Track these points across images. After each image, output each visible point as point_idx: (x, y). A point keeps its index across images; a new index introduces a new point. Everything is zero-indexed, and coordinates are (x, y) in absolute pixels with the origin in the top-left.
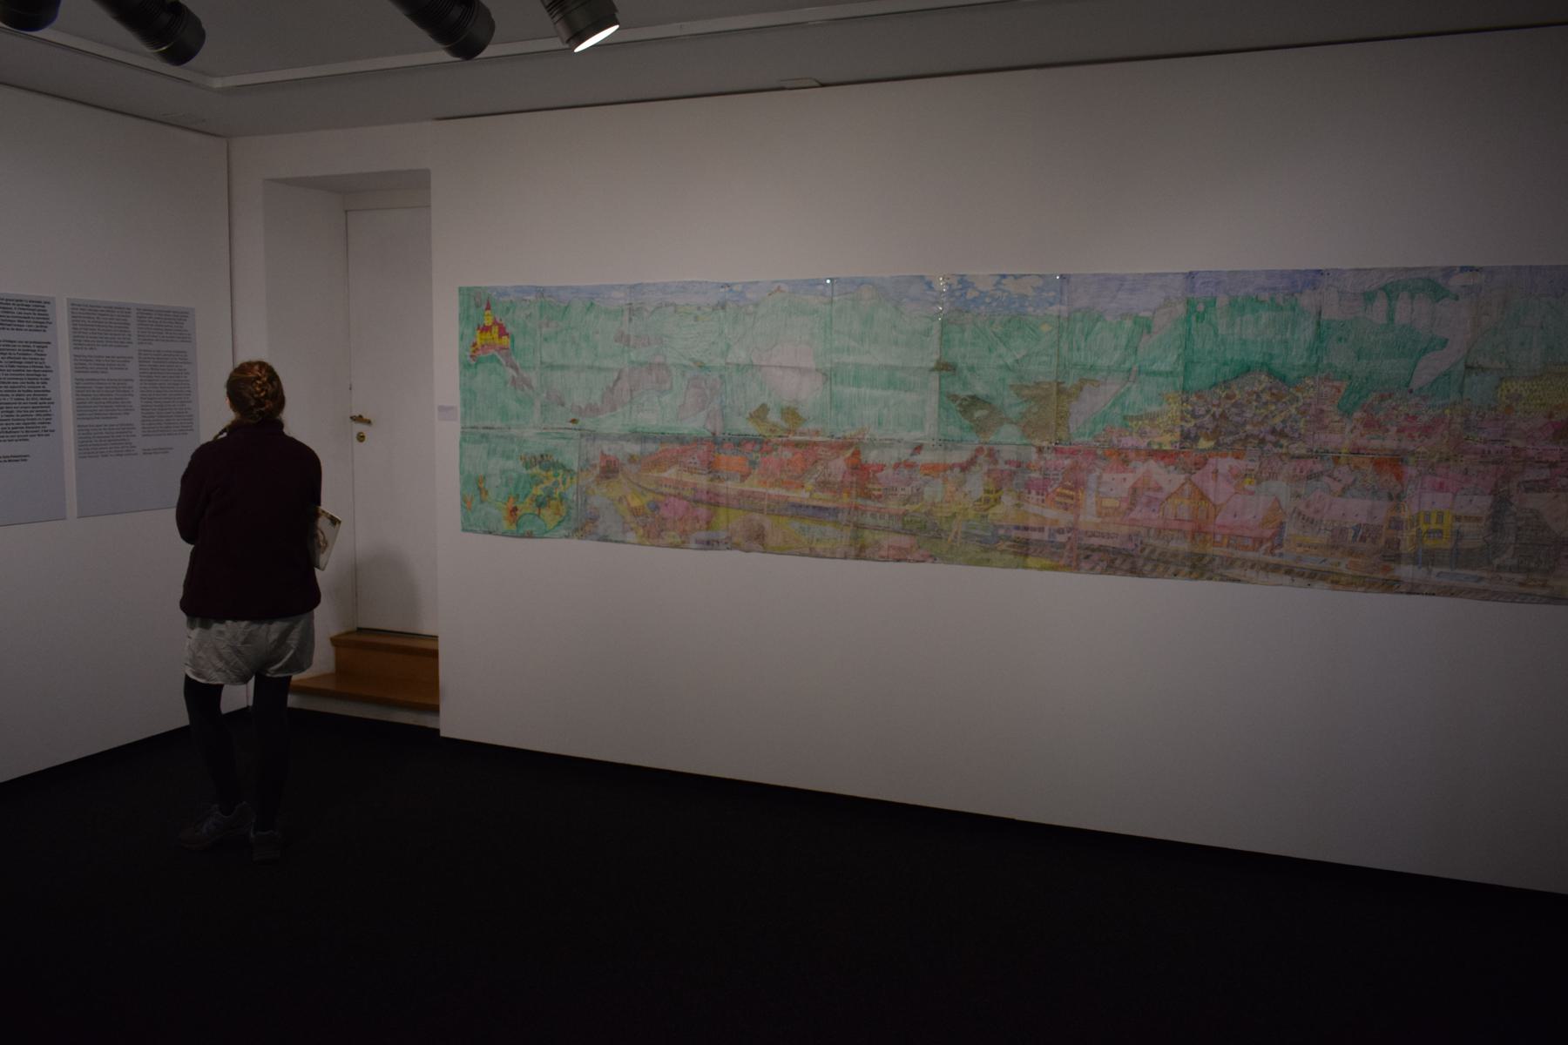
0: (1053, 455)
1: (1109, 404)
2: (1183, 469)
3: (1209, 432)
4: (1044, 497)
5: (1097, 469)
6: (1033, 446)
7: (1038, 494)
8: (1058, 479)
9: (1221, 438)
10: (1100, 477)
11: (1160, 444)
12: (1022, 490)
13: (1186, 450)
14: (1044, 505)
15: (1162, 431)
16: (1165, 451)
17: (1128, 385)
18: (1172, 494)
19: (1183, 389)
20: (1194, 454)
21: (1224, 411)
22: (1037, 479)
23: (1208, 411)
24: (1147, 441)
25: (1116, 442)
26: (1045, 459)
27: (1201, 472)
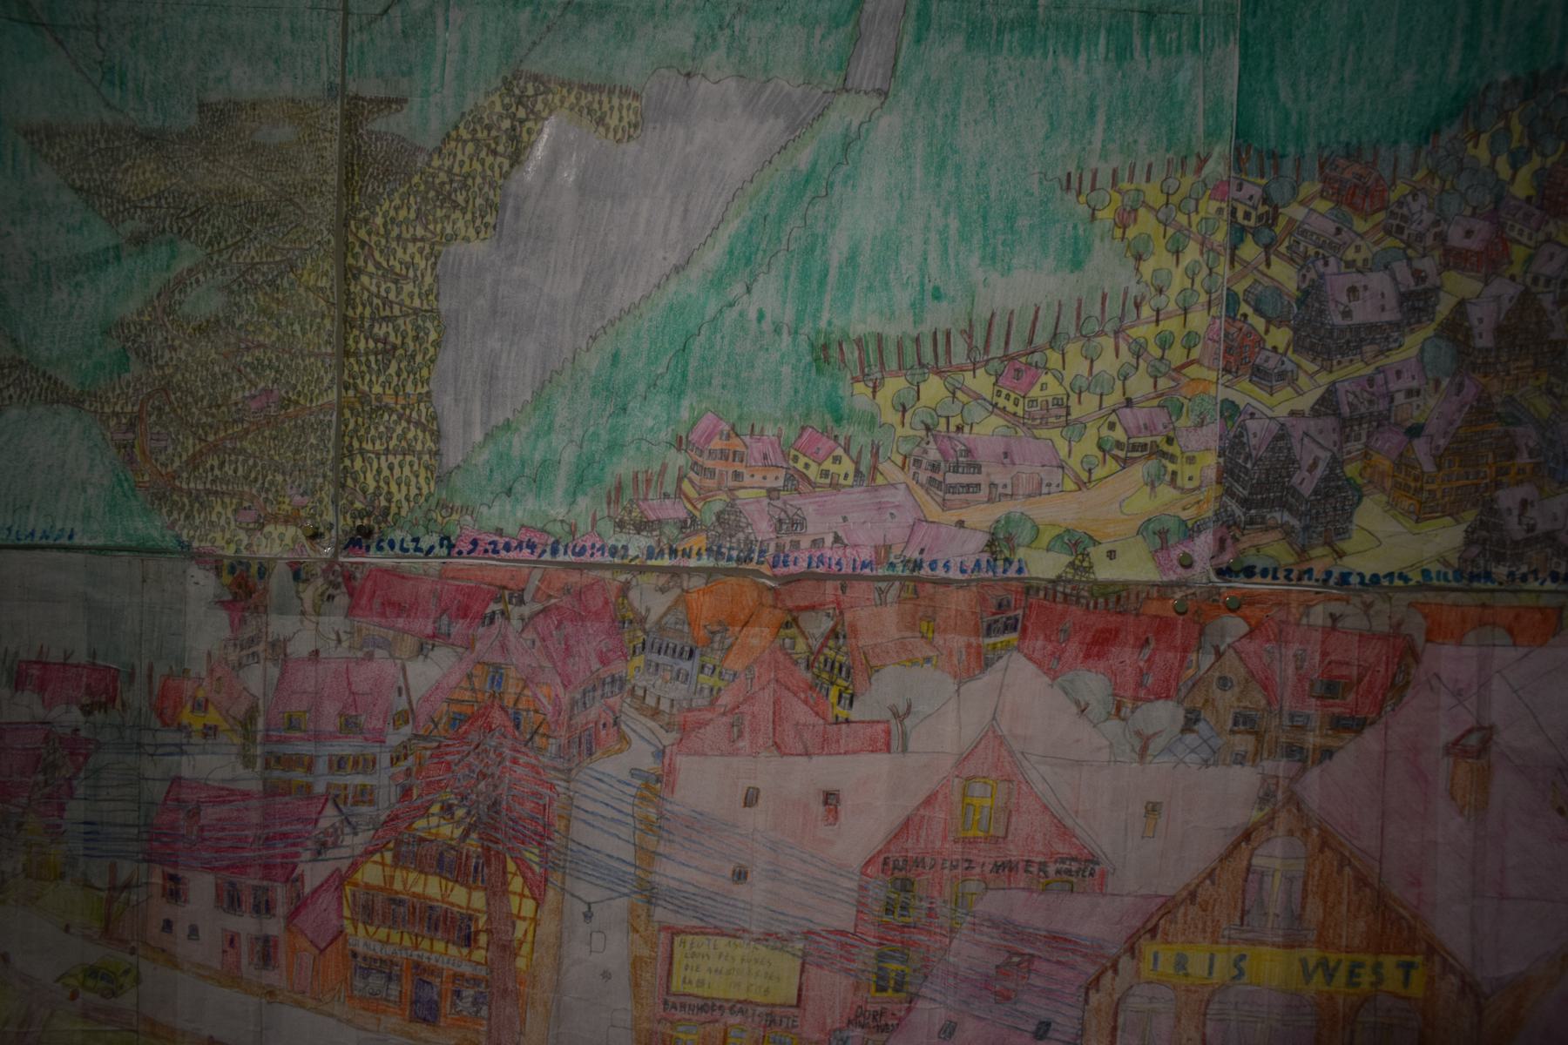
0: (335, 621)
1: (712, 257)
2: (1245, 722)
3: (1421, 449)
4: (274, 927)
5: (637, 725)
6: (199, 558)
7: (230, 900)
8: (365, 795)
9: (1508, 498)
10: (656, 784)
11: (1076, 544)
12: (126, 870)
13: (1258, 586)
14: (272, 977)
15: (1088, 446)
16: (1117, 596)
17: (846, 113)
18: (1168, 907)
19: (1244, 134)
20: (1318, 615)
21: (1526, 297)
22: (224, 795)
23: (1416, 304)
24: (981, 516)
25: (763, 529)
26: (278, 648)
27: (1370, 739)
